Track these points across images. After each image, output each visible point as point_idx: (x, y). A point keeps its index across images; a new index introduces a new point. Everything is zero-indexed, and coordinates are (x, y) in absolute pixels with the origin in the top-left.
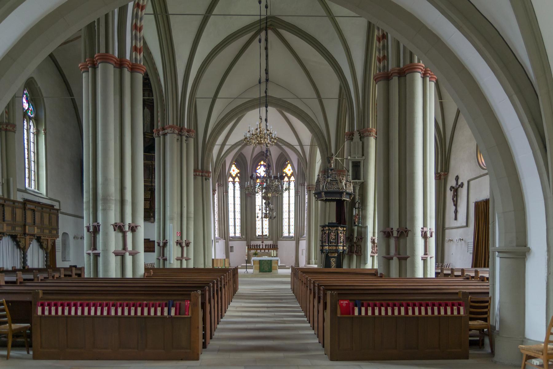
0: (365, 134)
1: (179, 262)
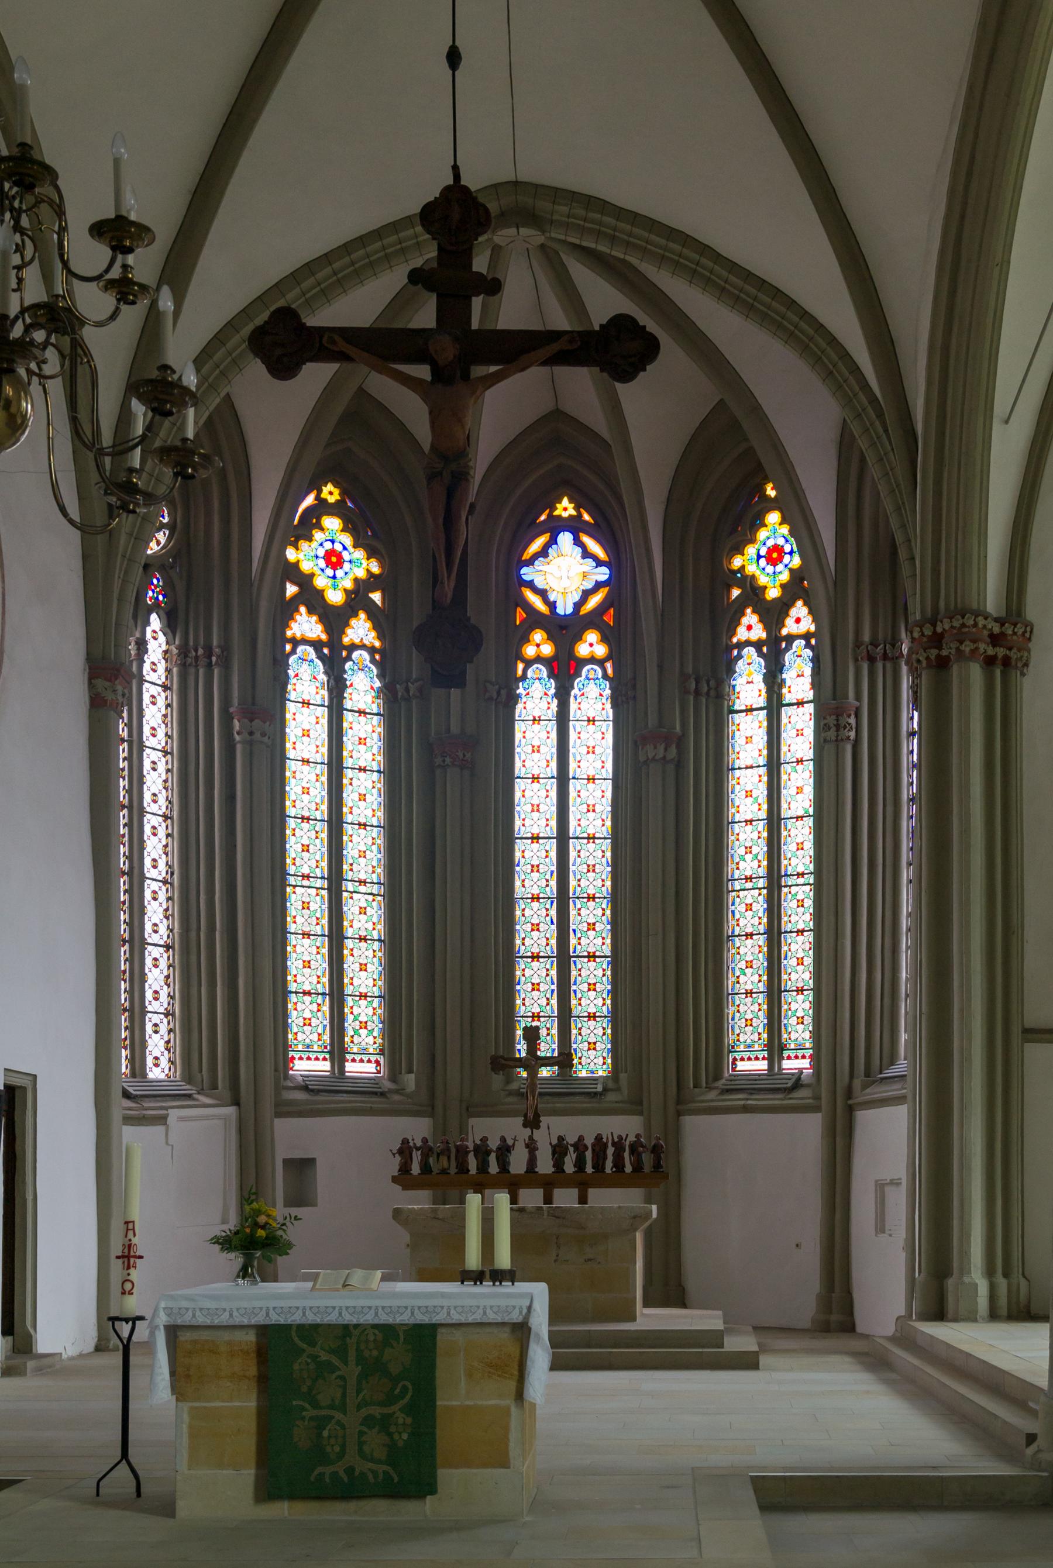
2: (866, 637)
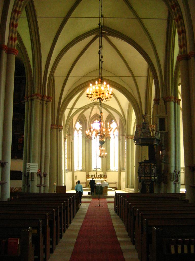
1: (38, 188)
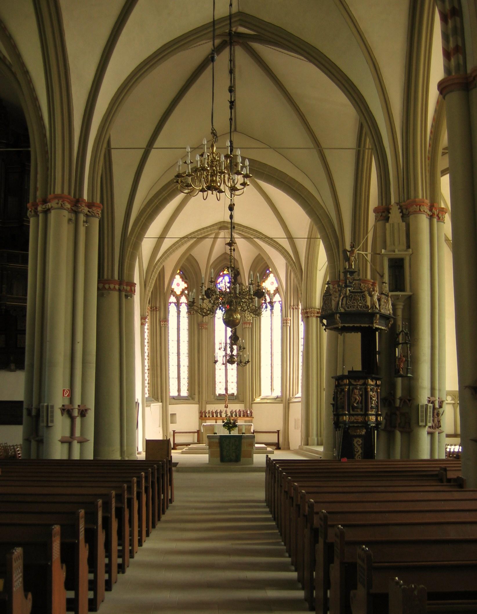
0: (411, 210)
1: (66, 446)
2: (292, 304)
